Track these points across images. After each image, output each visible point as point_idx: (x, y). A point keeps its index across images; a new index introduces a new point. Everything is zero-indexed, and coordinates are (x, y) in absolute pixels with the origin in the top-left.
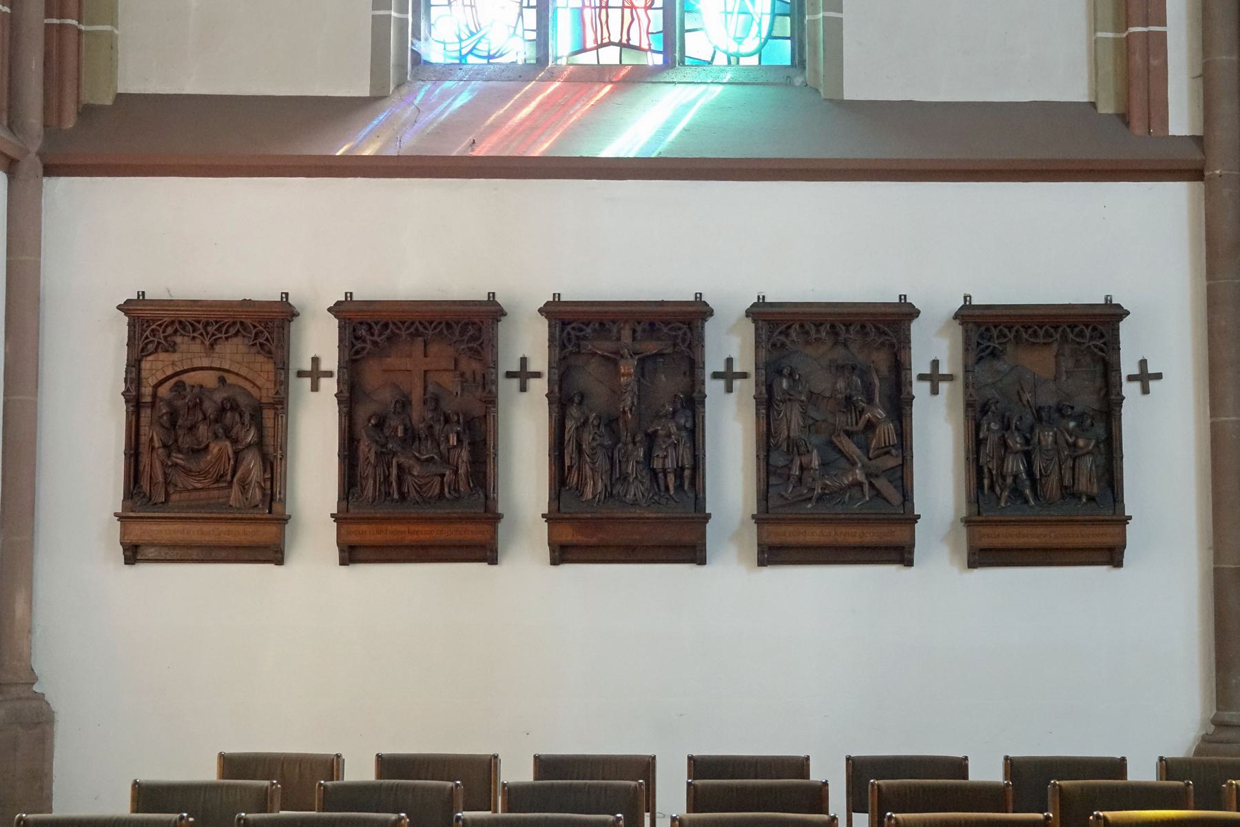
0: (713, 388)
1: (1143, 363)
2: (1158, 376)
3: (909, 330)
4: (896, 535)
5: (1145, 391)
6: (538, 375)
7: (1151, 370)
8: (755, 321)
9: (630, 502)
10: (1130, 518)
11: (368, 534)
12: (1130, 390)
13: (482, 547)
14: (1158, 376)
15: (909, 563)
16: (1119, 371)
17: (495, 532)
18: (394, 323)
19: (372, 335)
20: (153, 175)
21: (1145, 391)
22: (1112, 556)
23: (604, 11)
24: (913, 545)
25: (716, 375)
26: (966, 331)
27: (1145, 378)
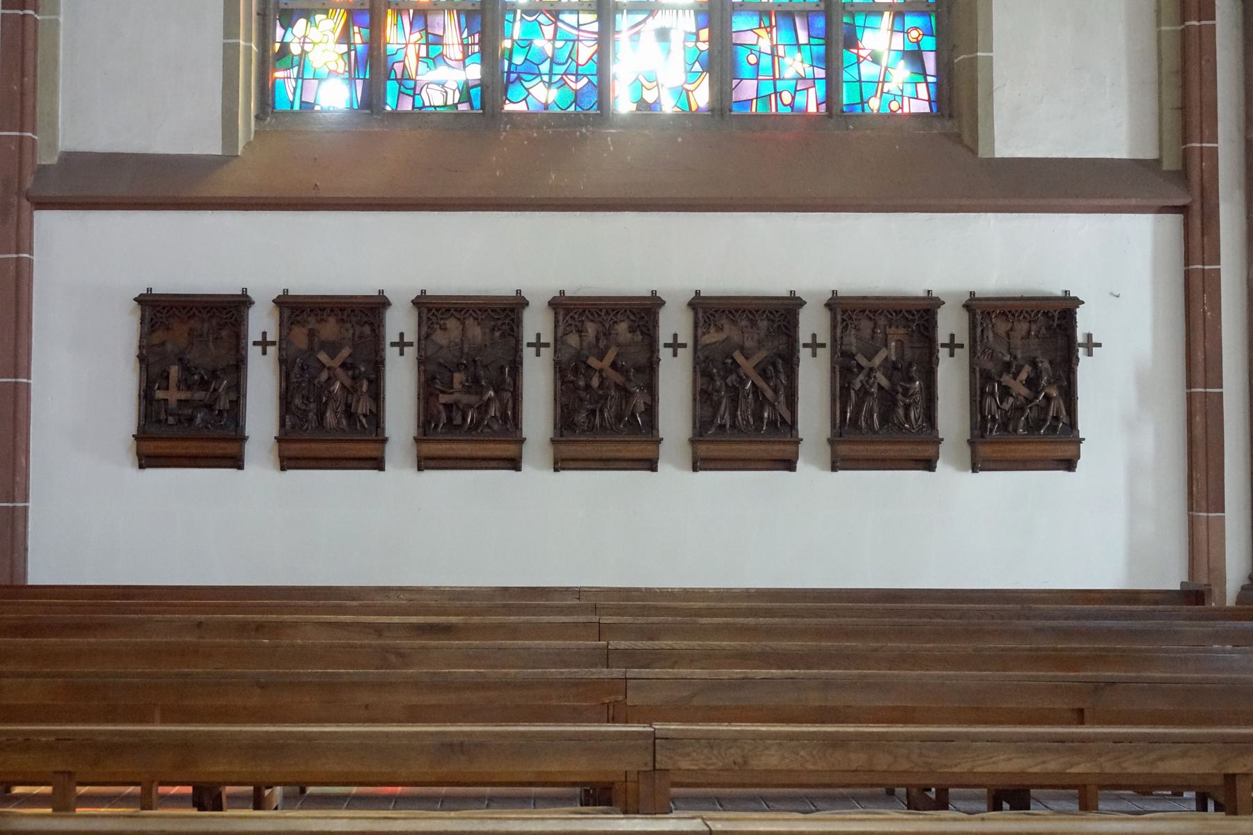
0: (665, 354)
2: (1099, 345)
4: (230, 448)
7: (1095, 340)
8: (419, 308)
9: (327, 428)
11: (295, 449)
13: (375, 459)
14: (1099, 345)
15: (241, 467)
16: (384, 338)
17: (383, 451)
20: (610, 210)
22: (1069, 464)
23: (300, 81)
25: (393, 344)
26: (143, 311)
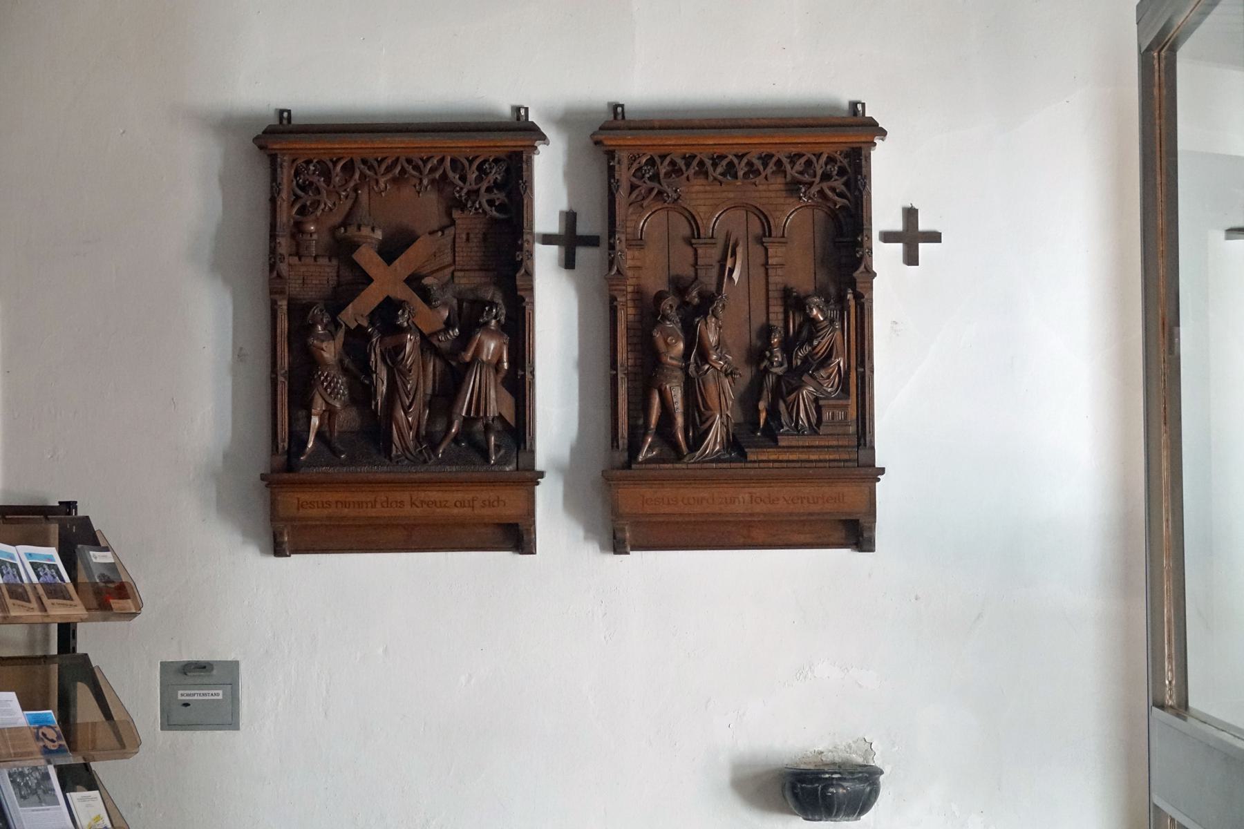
1: (910, 214)
2: (934, 237)
3: (225, 206)
5: (911, 258)
6: (888, 237)
10: (882, 471)
12: (885, 257)
14: (934, 237)
18: (364, 162)
19: (489, 190)
21: (911, 258)
24: (522, 553)
27: (912, 237)
